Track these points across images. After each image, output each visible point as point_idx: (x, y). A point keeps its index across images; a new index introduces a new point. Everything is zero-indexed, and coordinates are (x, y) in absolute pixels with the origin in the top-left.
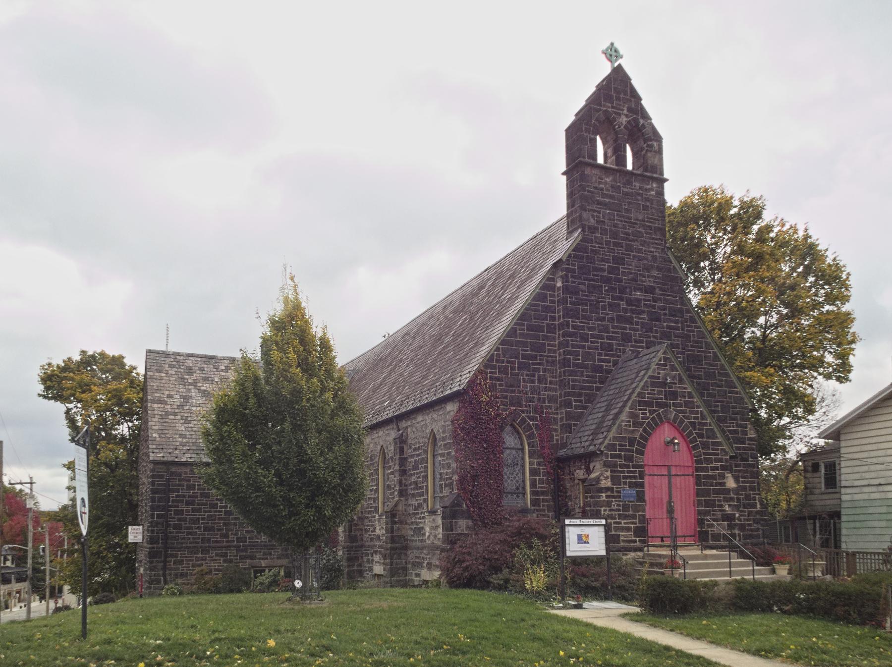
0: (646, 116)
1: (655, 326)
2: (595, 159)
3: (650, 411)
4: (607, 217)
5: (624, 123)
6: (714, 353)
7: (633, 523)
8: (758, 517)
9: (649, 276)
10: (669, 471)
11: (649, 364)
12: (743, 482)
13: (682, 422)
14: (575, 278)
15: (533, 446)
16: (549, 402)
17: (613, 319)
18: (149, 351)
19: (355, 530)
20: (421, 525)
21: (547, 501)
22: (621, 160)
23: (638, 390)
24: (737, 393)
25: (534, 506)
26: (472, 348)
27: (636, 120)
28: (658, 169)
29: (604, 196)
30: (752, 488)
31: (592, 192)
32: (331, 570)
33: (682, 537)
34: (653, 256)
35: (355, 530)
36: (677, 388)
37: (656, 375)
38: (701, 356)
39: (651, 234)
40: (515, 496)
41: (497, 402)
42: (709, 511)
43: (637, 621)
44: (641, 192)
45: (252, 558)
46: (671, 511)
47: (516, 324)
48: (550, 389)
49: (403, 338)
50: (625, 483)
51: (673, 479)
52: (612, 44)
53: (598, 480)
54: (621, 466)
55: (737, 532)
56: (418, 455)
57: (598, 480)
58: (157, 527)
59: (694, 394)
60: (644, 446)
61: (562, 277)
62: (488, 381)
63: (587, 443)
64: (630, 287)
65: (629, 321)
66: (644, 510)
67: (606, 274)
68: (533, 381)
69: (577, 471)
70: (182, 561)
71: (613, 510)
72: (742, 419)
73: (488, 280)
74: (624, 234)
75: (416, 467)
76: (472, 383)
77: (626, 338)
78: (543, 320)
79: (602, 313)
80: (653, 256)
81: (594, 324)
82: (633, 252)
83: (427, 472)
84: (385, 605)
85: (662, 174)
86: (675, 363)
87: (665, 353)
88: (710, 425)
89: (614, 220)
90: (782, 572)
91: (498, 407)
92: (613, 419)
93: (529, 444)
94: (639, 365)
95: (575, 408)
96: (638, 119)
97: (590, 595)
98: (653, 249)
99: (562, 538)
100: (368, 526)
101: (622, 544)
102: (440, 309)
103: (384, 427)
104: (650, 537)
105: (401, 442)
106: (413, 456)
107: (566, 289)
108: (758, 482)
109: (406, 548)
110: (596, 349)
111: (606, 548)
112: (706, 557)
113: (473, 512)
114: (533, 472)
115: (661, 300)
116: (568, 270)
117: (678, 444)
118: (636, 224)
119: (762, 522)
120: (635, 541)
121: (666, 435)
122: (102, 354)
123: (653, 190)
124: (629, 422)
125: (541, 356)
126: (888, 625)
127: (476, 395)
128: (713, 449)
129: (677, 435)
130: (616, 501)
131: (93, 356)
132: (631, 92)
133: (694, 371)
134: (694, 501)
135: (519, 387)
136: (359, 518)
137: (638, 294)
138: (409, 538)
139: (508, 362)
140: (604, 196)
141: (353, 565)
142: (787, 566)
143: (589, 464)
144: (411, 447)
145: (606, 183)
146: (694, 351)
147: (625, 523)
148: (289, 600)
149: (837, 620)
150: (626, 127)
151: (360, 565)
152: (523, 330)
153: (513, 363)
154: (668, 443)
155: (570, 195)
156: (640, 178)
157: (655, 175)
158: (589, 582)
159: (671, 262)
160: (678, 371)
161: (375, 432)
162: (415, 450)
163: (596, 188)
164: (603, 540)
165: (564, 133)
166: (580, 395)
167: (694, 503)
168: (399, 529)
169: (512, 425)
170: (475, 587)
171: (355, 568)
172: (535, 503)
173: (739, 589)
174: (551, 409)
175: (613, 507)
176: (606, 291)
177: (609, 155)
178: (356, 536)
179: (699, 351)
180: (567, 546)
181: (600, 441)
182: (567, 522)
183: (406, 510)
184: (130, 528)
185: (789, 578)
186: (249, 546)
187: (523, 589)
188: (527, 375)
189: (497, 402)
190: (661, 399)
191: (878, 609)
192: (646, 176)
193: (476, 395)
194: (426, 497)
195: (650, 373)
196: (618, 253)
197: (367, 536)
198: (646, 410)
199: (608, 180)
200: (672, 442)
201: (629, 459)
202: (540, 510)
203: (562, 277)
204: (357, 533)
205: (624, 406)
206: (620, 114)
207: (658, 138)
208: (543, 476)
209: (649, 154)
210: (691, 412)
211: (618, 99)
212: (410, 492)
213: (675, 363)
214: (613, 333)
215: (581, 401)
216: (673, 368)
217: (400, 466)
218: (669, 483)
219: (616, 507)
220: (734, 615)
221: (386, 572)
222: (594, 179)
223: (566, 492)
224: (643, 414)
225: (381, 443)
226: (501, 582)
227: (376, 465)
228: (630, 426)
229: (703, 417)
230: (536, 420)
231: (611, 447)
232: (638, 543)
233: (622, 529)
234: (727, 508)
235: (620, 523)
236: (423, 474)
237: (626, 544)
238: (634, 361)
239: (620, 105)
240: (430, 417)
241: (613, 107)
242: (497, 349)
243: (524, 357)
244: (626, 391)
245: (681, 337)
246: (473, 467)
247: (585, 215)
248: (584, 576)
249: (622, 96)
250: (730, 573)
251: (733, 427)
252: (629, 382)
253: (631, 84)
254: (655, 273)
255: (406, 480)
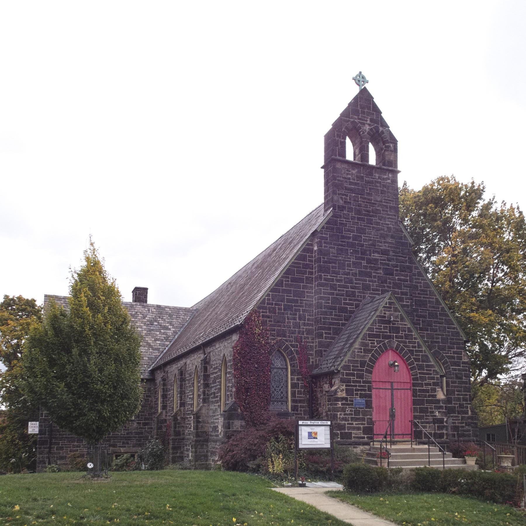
0: (384, 125)
1: (389, 279)
2: (344, 156)
3: (377, 341)
4: (352, 199)
5: (367, 130)
6: (437, 299)
7: (362, 424)
8: (470, 421)
9: (385, 242)
10: (392, 386)
11: (378, 306)
12: (458, 395)
13: (403, 349)
14: (327, 244)
15: (294, 366)
16: (307, 334)
17: (356, 274)
18: (46, 296)
19: (179, 427)
20: (217, 425)
21: (303, 407)
22: (365, 156)
23: (369, 326)
24: (454, 328)
25: (294, 411)
26: (256, 293)
27: (377, 129)
28: (394, 163)
29: (351, 183)
30: (465, 400)
31: (342, 181)
32: (155, 456)
33: (402, 435)
34: (388, 228)
35: (179, 427)
36: (399, 324)
37: (383, 315)
38: (426, 301)
39: (387, 211)
40: (280, 403)
41: (267, 334)
42: (423, 416)
43: (334, 497)
44: (380, 180)
45: (114, 446)
46: (392, 416)
47: (282, 277)
48: (308, 325)
49: (227, 286)
50: (357, 394)
51: (395, 392)
52: (360, 73)
53: (336, 392)
54: (354, 382)
55: (445, 432)
56: (216, 373)
57: (336, 392)
58: (44, 422)
59: (412, 329)
60: (372, 367)
61: (317, 243)
62: (261, 318)
63: (331, 365)
64: (370, 251)
65: (369, 275)
66: (371, 415)
67: (351, 240)
68: (295, 319)
69: (325, 385)
70: (63, 447)
71: (347, 414)
72: (457, 348)
73: (279, 245)
74: (365, 211)
75: (214, 382)
76: (248, 319)
77: (366, 288)
78: (304, 274)
79: (347, 269)
80: (388, 228)
81: (341, 277)
82: (372, 224)
83: (221, 385)
84: (163, 481)
85: (396, 166)
86: (397, 306)
87: (390, 299)
88: (425, 352)
89: (358, 201)
90: (471, 462)
91: (268, 337)
92: (349, 347)
93: (291, 365)
94: (372, 307)
95: (326, 339)
96: (378, 127)
97: (318, 477)
98: (389, 223)
99: (333, 436)
100: (187, 424)
101: (353, 439)
102: (250, 266)
103: (198, 352)
104: (375, 435)
105: (206, 362)
106: (213, 373)
107: (320, 251)
108: (470, 395)
109: (207, 441)
110: (342, 295)
111: (331, 442)
112: (414, 450)
113: (246, 415)
114: (294, 386)
115: (393, 259)
116: (322, 238)
117: (398, 366)
118: (376, 204)
119: (472, 425)
120: (364, 438)
121: (390, 360)
122: (20, 298)
123: (389, 179)
124: (361, 349)
125: (301, 300)
126: (523, 504)
127: (251, 328)
128: (427, 370)
129: (397, 358)
130: (349, 407)
131: (13, 299)
132: (373, 107)
133: (420, 312)
134: (411, 408)
135: (284, 323)
136: (182, 418)
137: (376, 256)
138: (210, 433)
139: (276, 304)
140: (351, 183)
141: (177, 453)
142: (475, 459)
143: (331, 381)
144: (212, 367)
145: (352, 174)
146: (420, 297)
147: (356, 424)
148: (84, 477)
149: (485, 499)
150: (368, 133)
151: (182, 453)
152: (288, 281)
153: (281, 305)
154: (391, 365)
155: (326, 183)
156: (379, 170)
157: (390, 168)
158: (318, 467)
159: (403, 232)
160: (399, 312)
161: (192, 355)
162: (215, 369)
163: (345, 178)
164: (329, 437)
165: (324, 138)
166: (330, 329)
167: (411, 410)
168: (202, 427)
169: (278, 350)
170: (237, 471)
171: (178, 455)
172: (294, 408)
173: (418, 474)
174: (309, 339)
175: (347, 412)
176: (352, 253)
177: (357, 153)
178: (179, 431)
179: (424, 297)
180: (300, 441)
181: (338, 363)
182: (300, 423)
183: (208, 413)
184: (30, 423)
185: (476, 468)
186: (112, 437)
187: (267, 472)
188: (290, 314)
189: (267, 334)
190: (387, 332)
191: (515, 492)
192: (384, 169)
193: (251, 328)
194: (219, 404)
195: (378, 313)
196: (361, 225)
197: (187, 431)
198: (374, 340)
199: (354, 172)
200: (393, 365)
201: (361, 376)
202: (298, 414)
203: (317, 243)
204: (180, 429)
205: (357, 337)
206: (364, 124)
207: (394, 141)
208: (301, 388)
209: (386, 153)
210: (410, 342)
211: (363, 113)
212: (211, 400)
213: (397, 306)
214: (356, 284)
215: (330, 334)
216: (396, 310)
217: (204, 381)
218: (392, 395)
219: (349, 412)
220: (413, 494)
221: (192, 458)
222: (343, 171)
223: (317, 401)
224: (371, 343)
225: (196, 364)
226: (254, 467)
227: (192, 380)
228: (361, 352)
229: (419, 346)
230: (297, 347)
231: (346, 367)
232: (366, 439)
233: (354, 428)
234: (437, 414)
235: (353, 424)
236: (218, 387)
237: (357, 440)
238: (370, 305)
239: (365, 117)
240: (223, 345)
241: (359, 119)
242: (268, 295)
243: (289, 301)
244: (361, 326)
245: (410, 287)
246: (246, 382)
247: (335, 198)
248: (315, 462)
249: (366, 110)
250: (444, 462)
251: (451, 353)
252: (364, 320)
253: (373, 101)
254: (390, 240)
255: (209, 391)
